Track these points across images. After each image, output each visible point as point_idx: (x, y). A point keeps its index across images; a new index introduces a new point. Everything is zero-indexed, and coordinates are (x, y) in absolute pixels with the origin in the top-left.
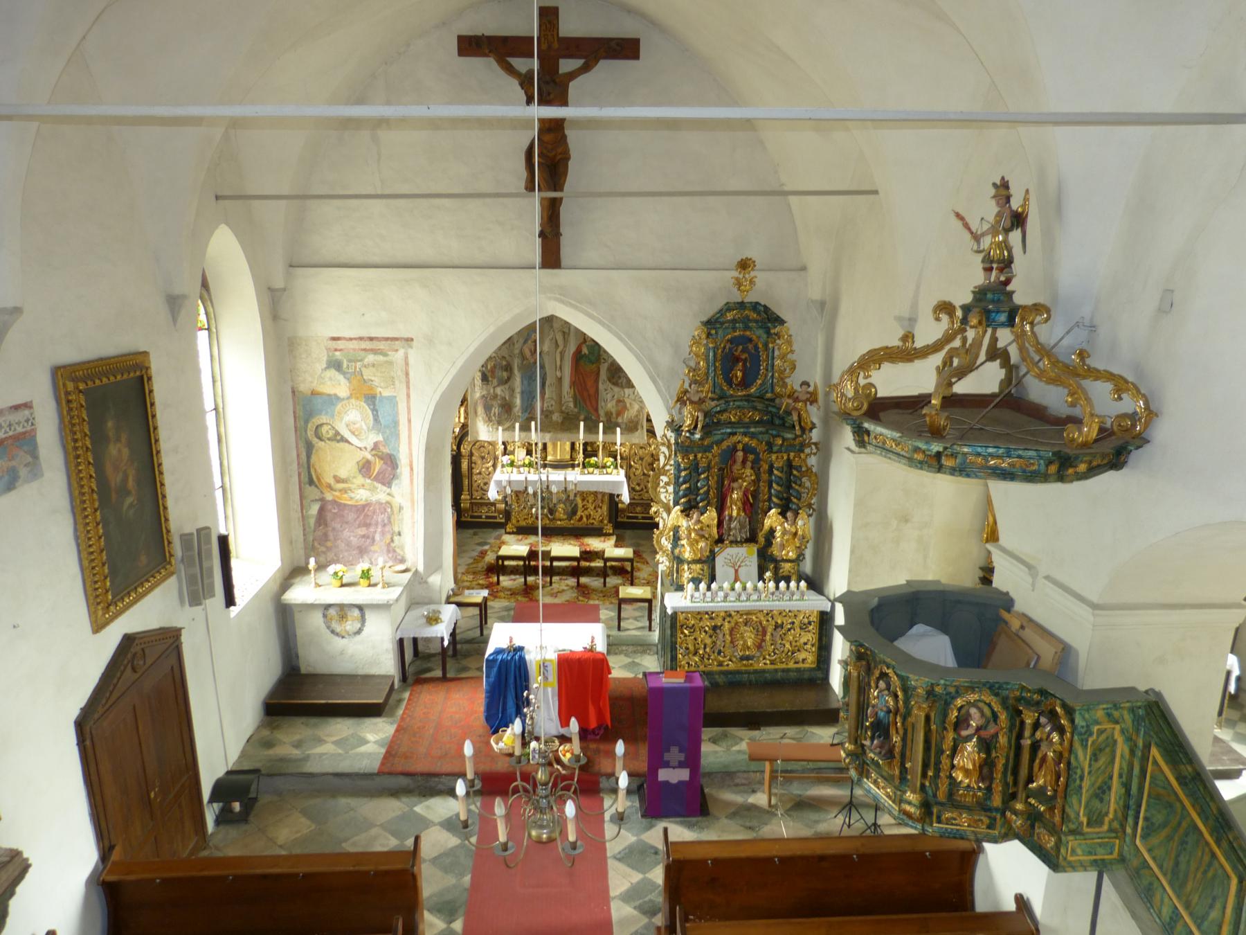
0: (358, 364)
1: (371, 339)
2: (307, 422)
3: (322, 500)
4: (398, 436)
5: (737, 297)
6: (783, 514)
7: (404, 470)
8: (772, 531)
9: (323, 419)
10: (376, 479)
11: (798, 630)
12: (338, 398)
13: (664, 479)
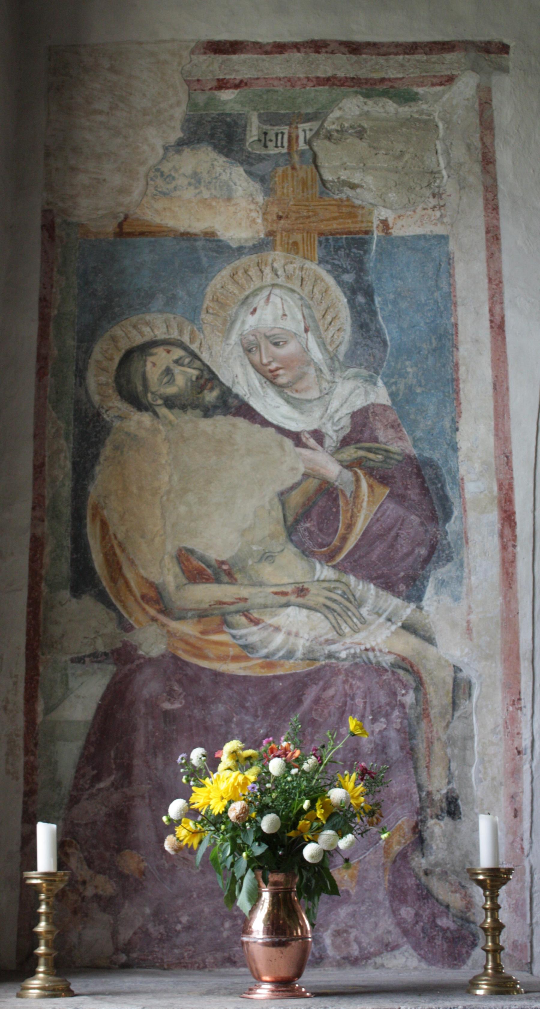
0: (304, 130)
1: (354, 48)
2: (88, 336)
3: (124, 656)
4: (449, 386)
9: (157, 324)
10: (356, 564)
12: (217, 249)
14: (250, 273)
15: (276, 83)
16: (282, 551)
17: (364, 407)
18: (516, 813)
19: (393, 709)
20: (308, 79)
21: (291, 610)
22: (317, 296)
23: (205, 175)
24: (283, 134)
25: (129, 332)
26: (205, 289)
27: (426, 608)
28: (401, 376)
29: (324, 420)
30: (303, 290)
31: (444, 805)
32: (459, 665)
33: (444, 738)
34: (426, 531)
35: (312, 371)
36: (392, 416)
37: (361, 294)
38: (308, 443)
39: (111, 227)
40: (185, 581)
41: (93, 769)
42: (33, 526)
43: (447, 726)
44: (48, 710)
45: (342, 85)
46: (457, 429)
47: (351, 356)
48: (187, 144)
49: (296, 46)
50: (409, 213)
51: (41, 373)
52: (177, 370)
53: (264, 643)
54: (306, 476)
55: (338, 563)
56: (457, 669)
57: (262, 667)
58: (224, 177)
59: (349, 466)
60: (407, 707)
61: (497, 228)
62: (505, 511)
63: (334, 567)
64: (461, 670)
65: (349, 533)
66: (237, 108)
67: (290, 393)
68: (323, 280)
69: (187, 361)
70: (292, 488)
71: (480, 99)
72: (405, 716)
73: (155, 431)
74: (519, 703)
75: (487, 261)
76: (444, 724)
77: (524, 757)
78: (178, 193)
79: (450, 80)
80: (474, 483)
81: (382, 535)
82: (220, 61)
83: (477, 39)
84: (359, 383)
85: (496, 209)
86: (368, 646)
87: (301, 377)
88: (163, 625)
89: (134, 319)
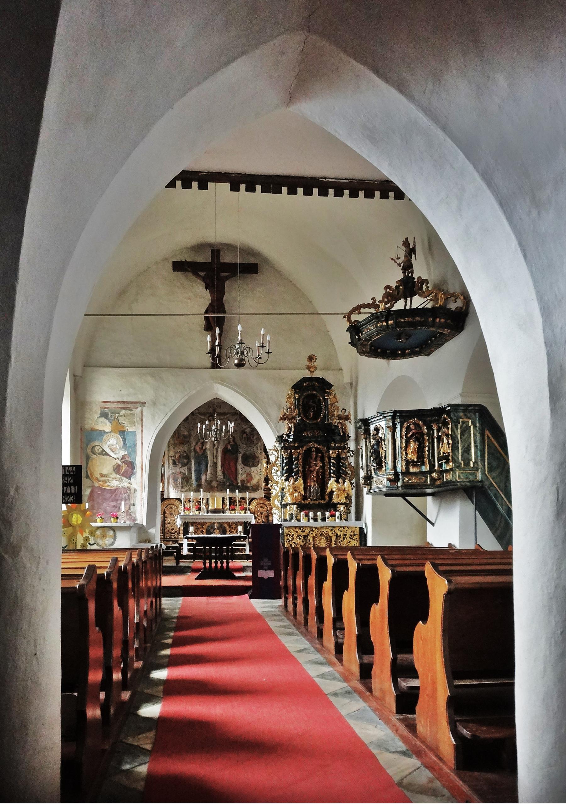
1: (124, 402)
2: (87, 445)
3: (93, 486)
4: (135, 452)
5: (307, 374)
6: (337, 481)
7: (138, 470)
8: (332, 492)
9: (97, 443)
10: (123, 475)
11: (349, 539)
13: (276, 468)
25: (93, 444)
37: (124, 439)
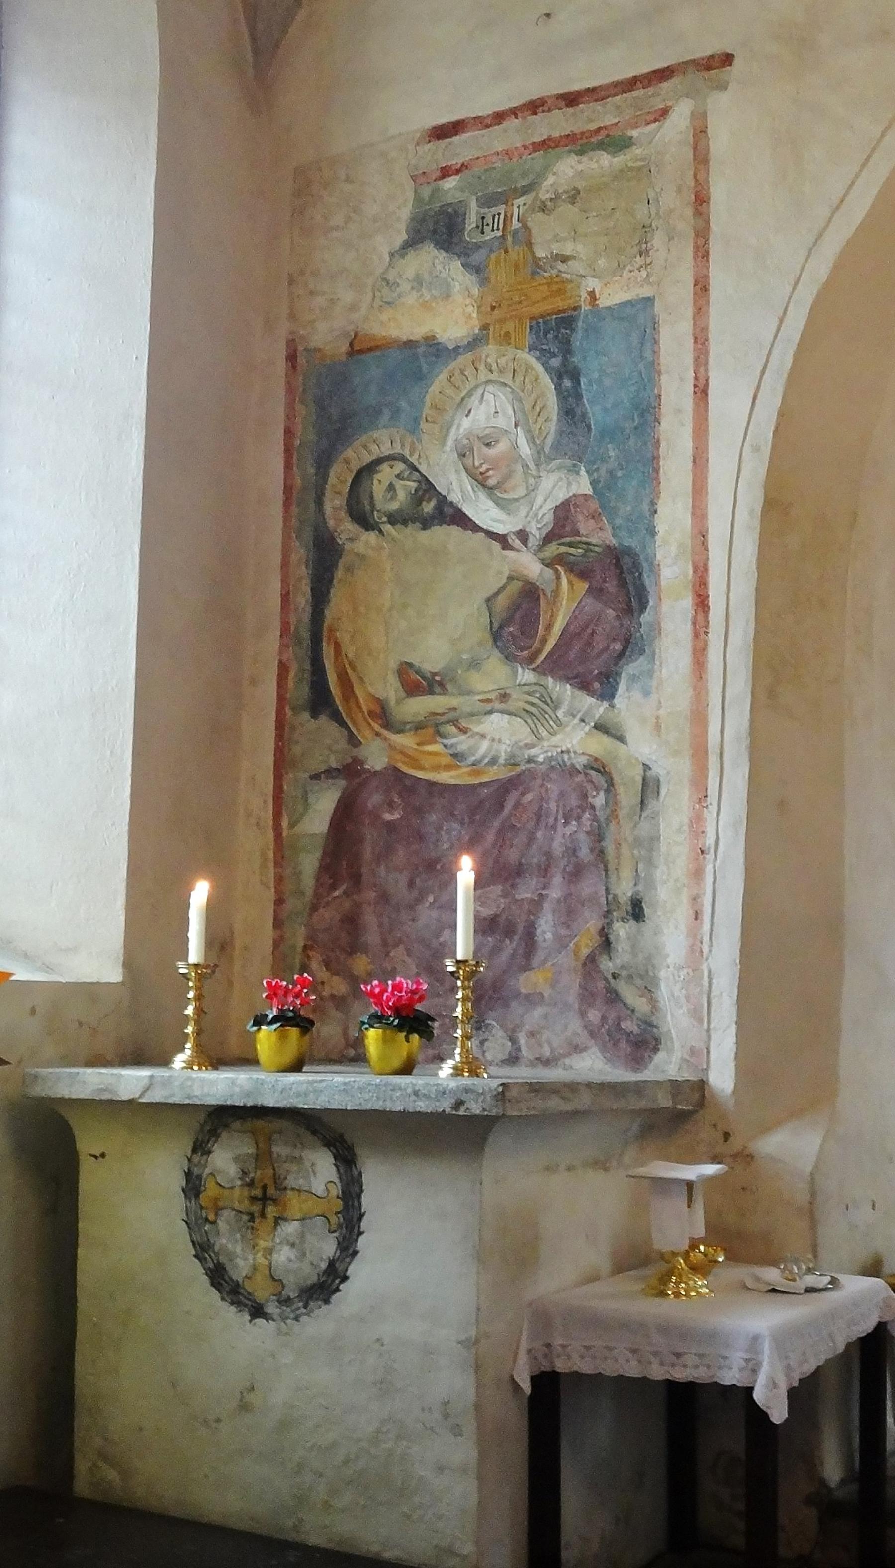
1: (571, 100)
3: (352, 771)
4: (649, 466)
9: (382, 440)
10: (557, 665)
12: (436, 350)
14: (466, 373)
15: (494, 159)
16: (488, 658)
17: (566, 500)
18: (697, 916)
19: (584, 811)
20: (525, 147)
21: (495, 717)
22: (528, 387)
23: (426, 276)
24: (499, 214)
26: (424, 397)
27: (617, 706)
28: (603, 461)
29: (528, 518)
30: (514, 382)
31: (630, 908)
32: (648, 763)
33: (630, 839)
34: (622, 625)
35: (519, 468)
36: (594, 505)
37: (567, 376)
38: (515, 546)
39: (344, 348)
40: (404, 694)
41: (330, 878)
42: (281, 653)
43: (635, 826)
44: (292, 825)
45: (557, 146)
46: (656, 512)
47: (557, 446)
48: (411, 246)
49: (514, 112)
50: (615, 279)
51: (287, 504)
52: (399, 484)
53: (473, 750)
54: (510, 578)
55: (538, 666)
56: (646, 767)
57: (470, 774)
58: (444, 275)
59: (548, 564)
60: (597, 809)
61: (706, 277)
62: (699, 596)
63: (534, 670)
64: (650, 769)
65: (549, 634)
66: (459, 196)
67: (499, 495)
68: (533, 369)
69: (407, 474)
70: (497, 594)
71: (695, 130)
72: (595, 819)
73: (380, 548)
74: (706, 801)
75: (694, 319)
76: (632, 825)
77: (707, 856)
78: (403, 300)
79: (664, 113)
80: (670, 569)
81: (579, 634)
82: (443, 147)
83: (698, 55)
84: (562, 474)
85: (706, 255)
86: (564, 749)
87: (509, 476)
88: (386, 739)
89: (364, 438)
